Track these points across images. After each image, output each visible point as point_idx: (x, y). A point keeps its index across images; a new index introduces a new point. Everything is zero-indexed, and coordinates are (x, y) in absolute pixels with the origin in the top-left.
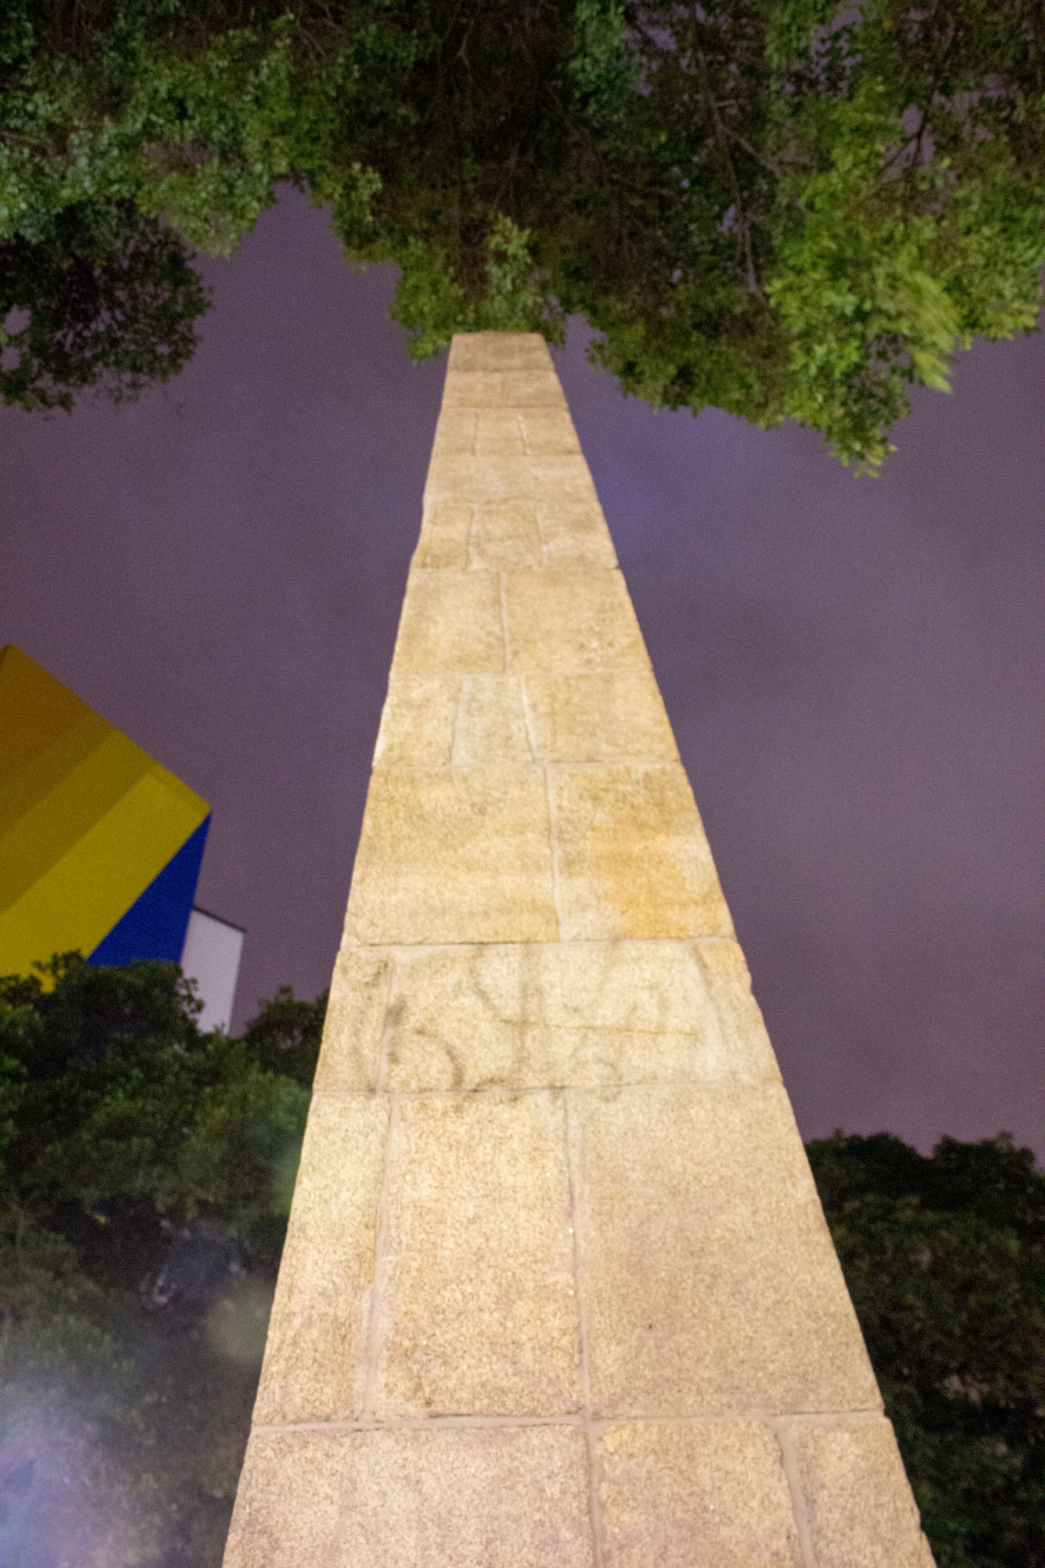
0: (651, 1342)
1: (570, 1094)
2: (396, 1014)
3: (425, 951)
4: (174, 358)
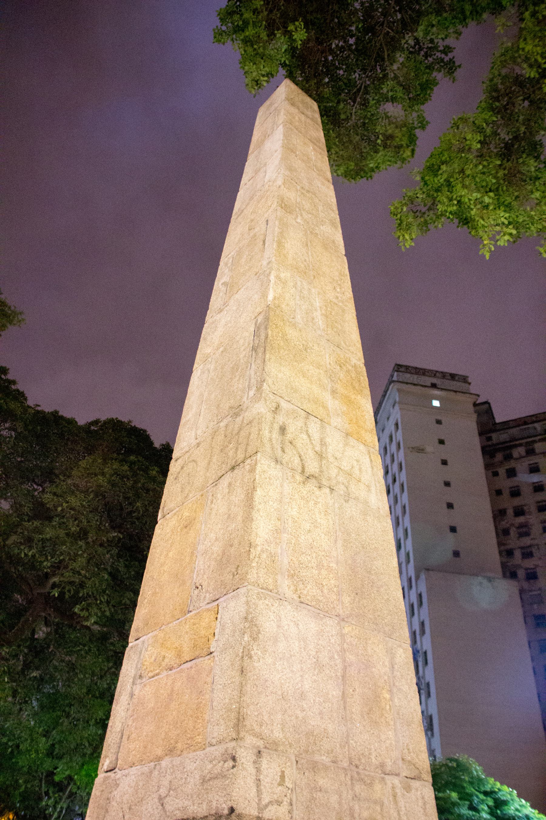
0: (357, 599)
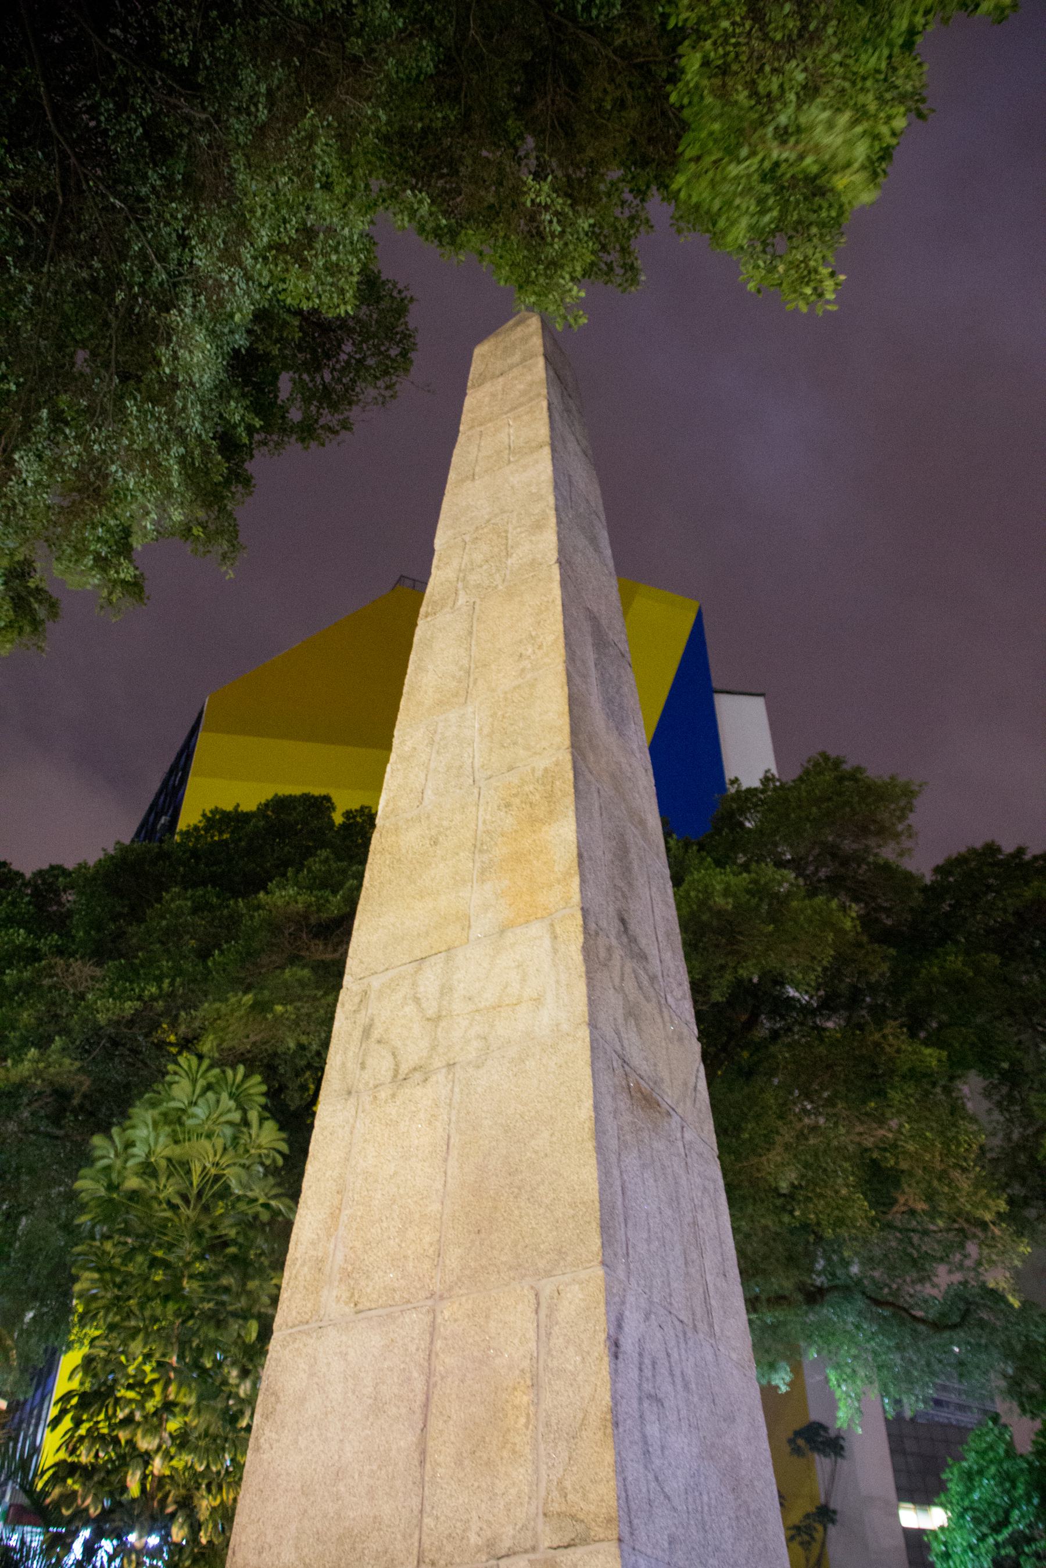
1: (458, 1066)
2: (367, 1032)
3: (391, 973)
4: (404, 354)
